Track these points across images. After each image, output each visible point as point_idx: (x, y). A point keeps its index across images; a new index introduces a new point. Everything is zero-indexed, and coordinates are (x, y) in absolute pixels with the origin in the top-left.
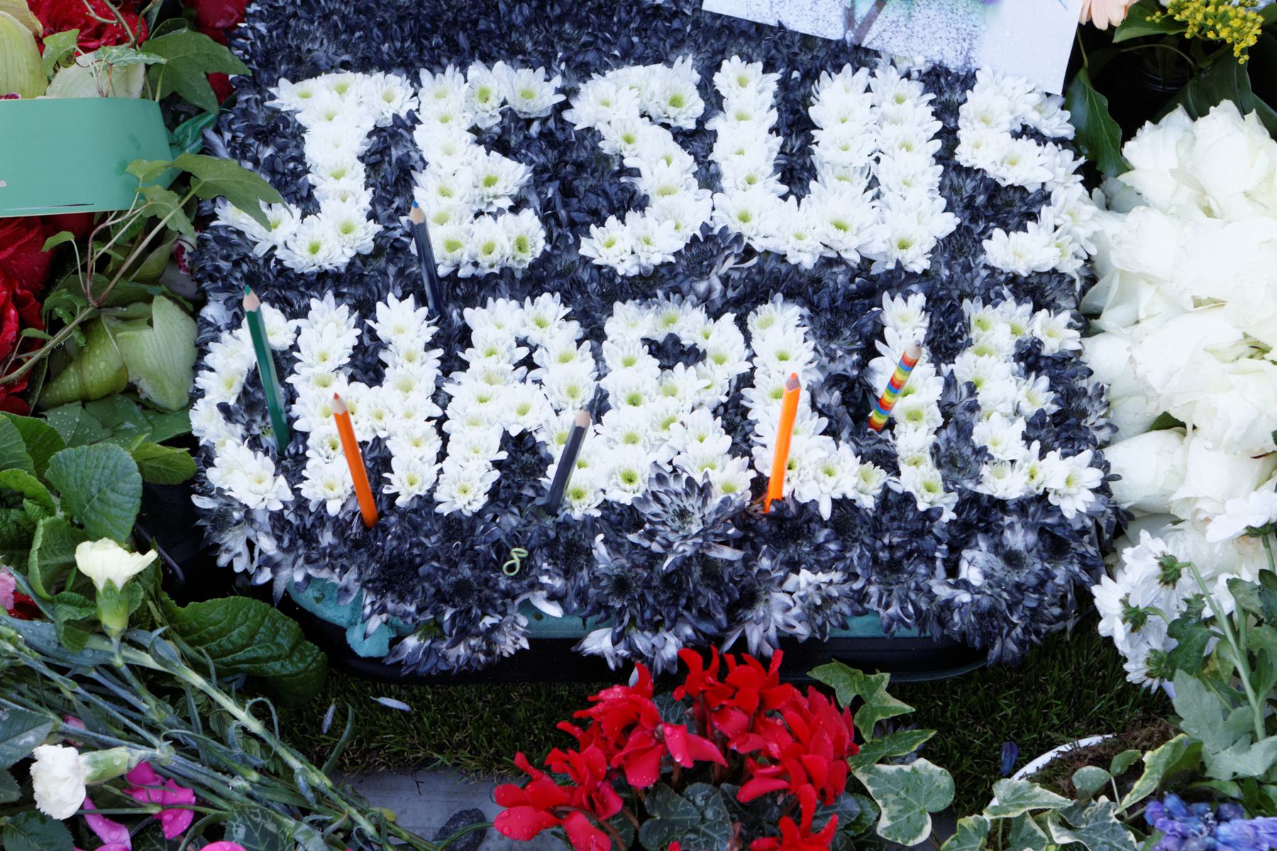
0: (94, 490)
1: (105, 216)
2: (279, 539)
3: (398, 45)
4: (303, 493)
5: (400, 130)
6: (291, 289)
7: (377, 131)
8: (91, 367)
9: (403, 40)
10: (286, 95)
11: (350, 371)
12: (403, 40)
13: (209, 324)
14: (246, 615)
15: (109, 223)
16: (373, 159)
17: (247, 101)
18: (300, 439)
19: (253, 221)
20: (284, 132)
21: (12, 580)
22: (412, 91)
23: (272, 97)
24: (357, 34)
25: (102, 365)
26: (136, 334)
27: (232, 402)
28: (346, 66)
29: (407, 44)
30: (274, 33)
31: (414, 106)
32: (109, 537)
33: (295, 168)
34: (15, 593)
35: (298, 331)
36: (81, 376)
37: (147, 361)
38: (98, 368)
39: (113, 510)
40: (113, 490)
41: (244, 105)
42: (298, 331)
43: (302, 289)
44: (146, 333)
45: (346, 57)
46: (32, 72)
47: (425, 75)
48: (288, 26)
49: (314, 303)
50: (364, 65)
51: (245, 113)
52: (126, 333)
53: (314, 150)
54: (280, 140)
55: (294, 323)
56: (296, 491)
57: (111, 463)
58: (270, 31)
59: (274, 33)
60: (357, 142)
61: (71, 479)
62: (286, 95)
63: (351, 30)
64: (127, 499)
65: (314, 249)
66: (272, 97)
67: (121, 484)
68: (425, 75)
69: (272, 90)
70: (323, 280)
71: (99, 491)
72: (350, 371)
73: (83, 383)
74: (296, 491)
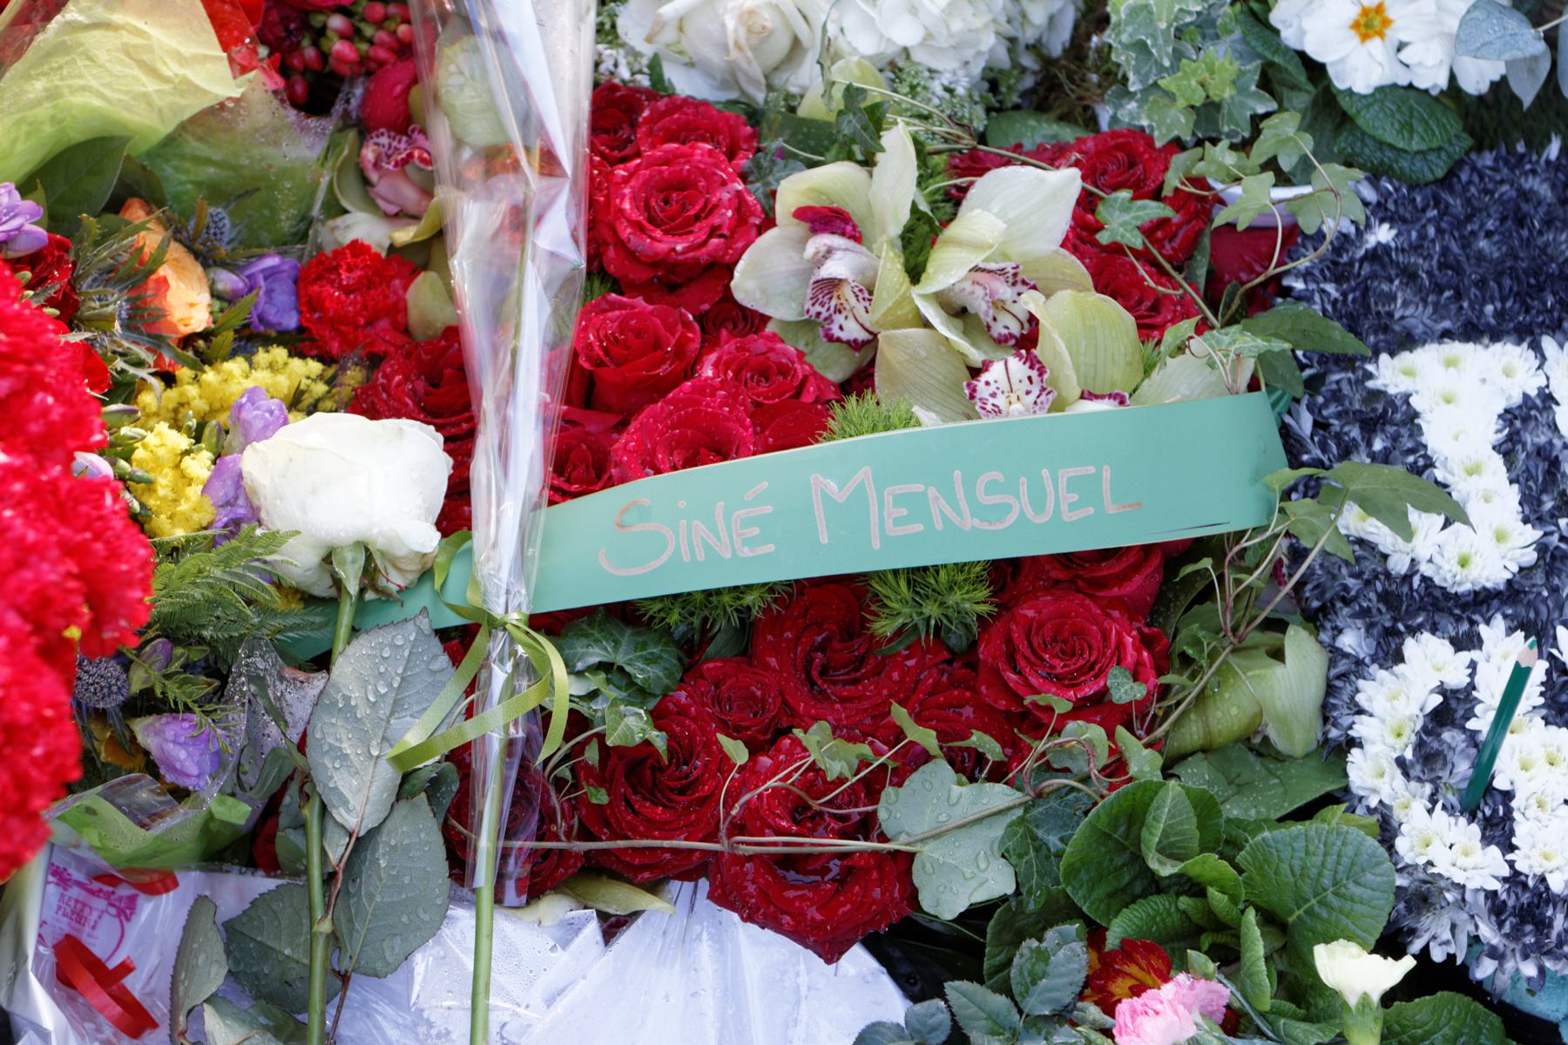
0: (1326, 882)
1: (1240, 535)
2: (1500, 924)
3: (1499, 305)
4: (1518, 867)
5: (1533, 412)
6: (1458, 612)
7: (1508, 416)
8: (1219, 714)
9: (1503, 300)
10: (1389, 374)
11: (1544, 712)
12: (1503, 300)
13: (1346, 655)
14: (1450, 1012)
15: (1244, 544)
16: (1504, 447)
17: (1338, 382)
18: (1499, 798)
19: (1385, 530)
20: (1392, 421)
21: (1227, 992)
22: (1537, 363)
23: (1370, 376)
24: (1447, 294)
25: (1234, 711)
26: (1269, 672)
27: (1409, 755)
28: (1446, 335)
29: (1509, 304)
30: (1350, 297)
31: (1543, 383)
32: (1349, 939)
33: (1416, 462)
34: (1228, 1007)
35: (1473, 665)
36: (1206, 725)
37: (1278, 704)
38: (1228, 714)
39: (1358, 908)
40: (1357, 883)
41: (1334, 387)
42: (1473, 665)
43: (1457, 611)
44: (1277, 671)
45: (1447, 324)
46: (1129, 364)
47: (1548, 343)
48: (1367, 288)
49: (1483, 629)
50: (1471, 332)
51: (1336, 396)
52: (1257, 672)
53: (1436, 435)
54: (1391, 429)
55: (1466, 656)
56: (1511, 864)
57: (1350, 850)
58: (1345, 295)
59: (1350, 297)
60: (1489, 431)
61: (1285, 867)
62: (1389, 374)
63: (1439, 289)
64: (1377, 894)
65: (1464, 563)
66: (1370, 376)
67: (1369, 877)
68: (1548, 343)
69: (1370, 367)
70: (1481, 602)
71: (1335, 883)
72: (1544, 712)
73: (1208, 733)
74: (1511, 864)
